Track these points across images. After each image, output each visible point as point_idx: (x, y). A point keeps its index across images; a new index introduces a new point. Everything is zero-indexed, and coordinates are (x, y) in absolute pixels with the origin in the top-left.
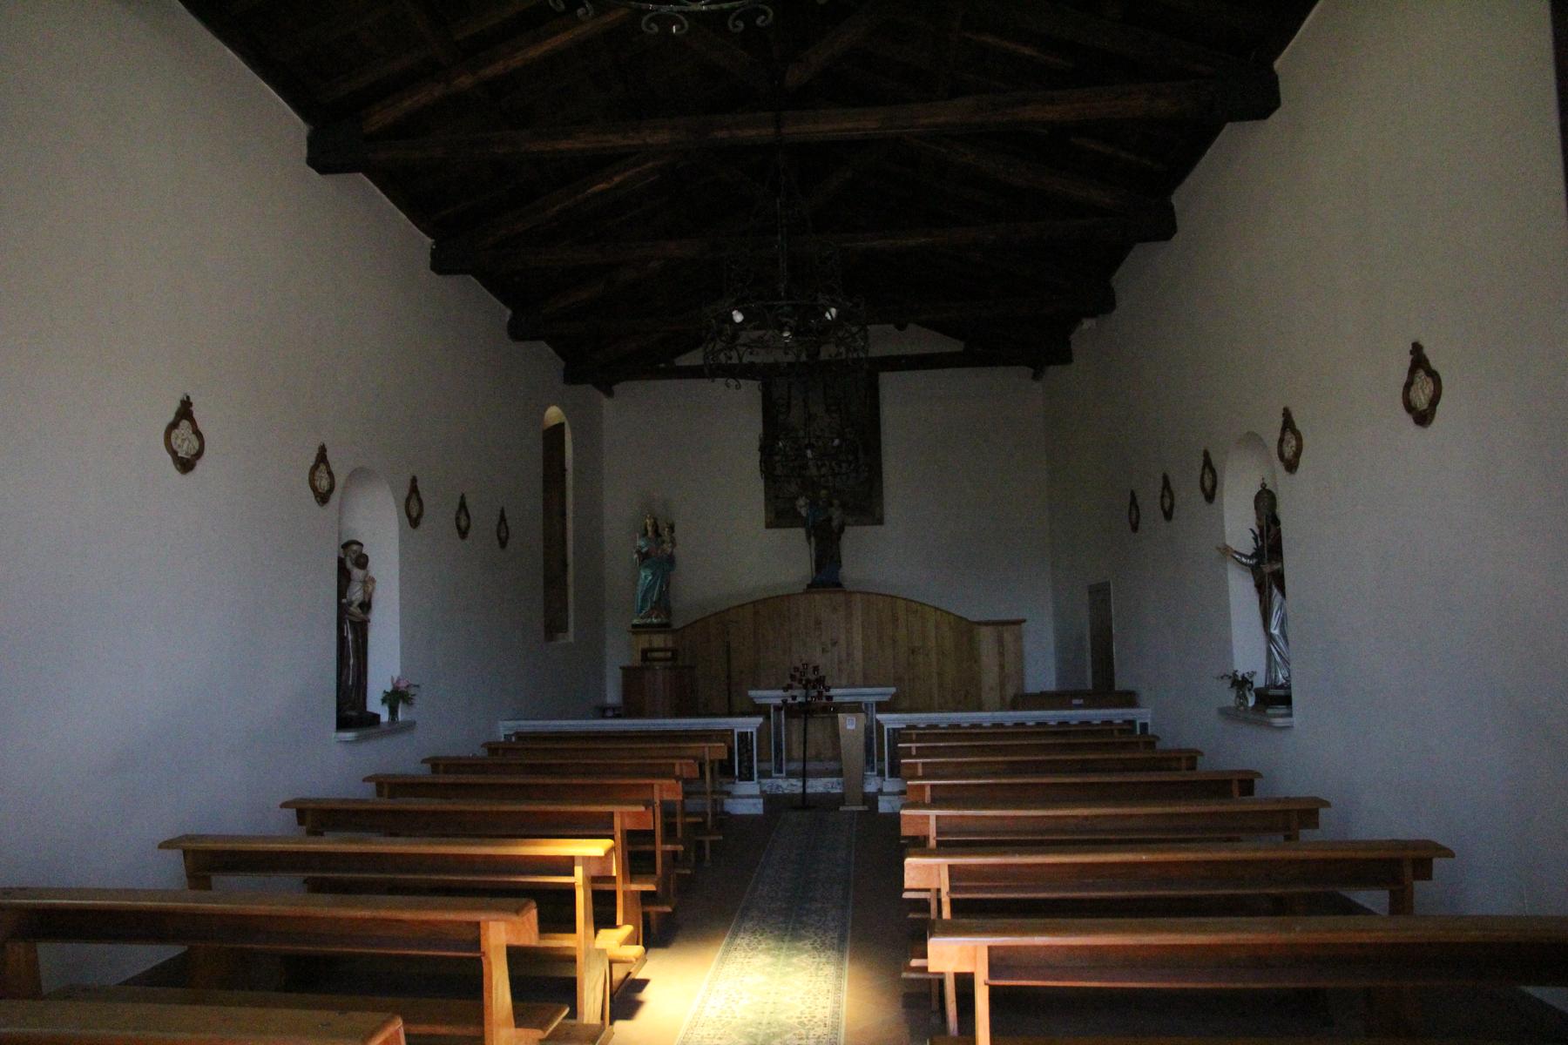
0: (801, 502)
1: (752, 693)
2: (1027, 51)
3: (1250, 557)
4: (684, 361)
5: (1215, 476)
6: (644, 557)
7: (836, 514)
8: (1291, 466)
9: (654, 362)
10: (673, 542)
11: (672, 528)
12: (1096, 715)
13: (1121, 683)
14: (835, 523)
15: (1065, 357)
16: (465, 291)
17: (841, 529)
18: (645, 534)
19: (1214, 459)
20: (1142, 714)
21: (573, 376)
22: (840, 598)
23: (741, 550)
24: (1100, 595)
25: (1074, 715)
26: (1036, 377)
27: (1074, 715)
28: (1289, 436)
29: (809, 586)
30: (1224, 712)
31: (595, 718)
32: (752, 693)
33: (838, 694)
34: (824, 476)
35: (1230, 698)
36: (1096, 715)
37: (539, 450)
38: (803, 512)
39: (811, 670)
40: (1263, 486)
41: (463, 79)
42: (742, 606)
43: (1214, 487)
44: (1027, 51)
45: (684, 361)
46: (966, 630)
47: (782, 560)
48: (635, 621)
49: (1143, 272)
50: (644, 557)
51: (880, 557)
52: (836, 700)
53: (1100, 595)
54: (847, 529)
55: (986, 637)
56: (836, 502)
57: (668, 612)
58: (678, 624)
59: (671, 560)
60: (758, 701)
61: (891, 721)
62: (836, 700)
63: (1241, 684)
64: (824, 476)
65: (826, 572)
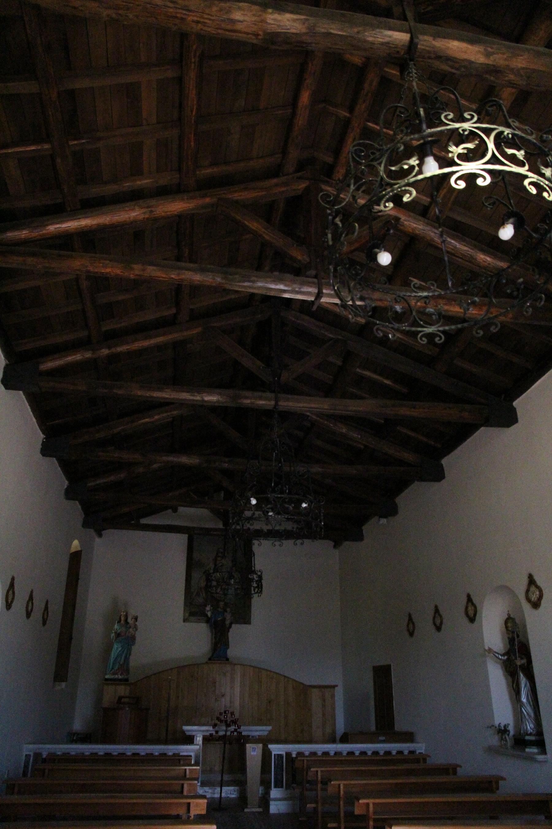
0: (208, 608)
1: (185, 728)
2: (387, 382)
3: (503, 655)
4: (144, 521)
5: (475, 607)
6: (118, 635)
7: (228, 617)
8: (536, 605)
9: (130, 521)
10: (136, 628)
11: (136, 619)
12: (381, 747)
13: (400, 726)
14: (228, 622)
15: (360, 538)
16: (52, 465)
17: (230, 627)
18: (119, 622)
19: (475, 600)
20: (420, 747)
21: (86, 524)
22: (228, 668)
23: (171, 635)
24: (382, 674)
25: (357, 747)
26: (335, 547)
27: (357, 747)
28: (533, 588)
29: (210, 659)
30: (490, 750)
31: (66, 743)
32: (185, 728)
33: (246, 730)
34: (221, 594)
35: (495, 740)
36: (381, 747)
37: (65, 565)
38: (209, 614)
39: (229, 715)
40: (509, 615)
41: (103, 350)
42: (171, 669)
43: (475, 615)
44: (387, 382)
45: (144, 521)
46: (303, 691)
47: (187, 640)
48: (107, 677)
49: (417, 498)
50: (118, 635)
51: (248, 642)
52: (243, 734)
53: (382, 674)
54: (233, 626)
55: (315, 697)
56: (228, 610)
57: (128, 671)
58: (132, 680)
59: (133, 638)
60: (188, 733)
61: (276, 749)
62: (243, 734)
63: (503, 731)
64: (221, 594)
65: (219, 650)
